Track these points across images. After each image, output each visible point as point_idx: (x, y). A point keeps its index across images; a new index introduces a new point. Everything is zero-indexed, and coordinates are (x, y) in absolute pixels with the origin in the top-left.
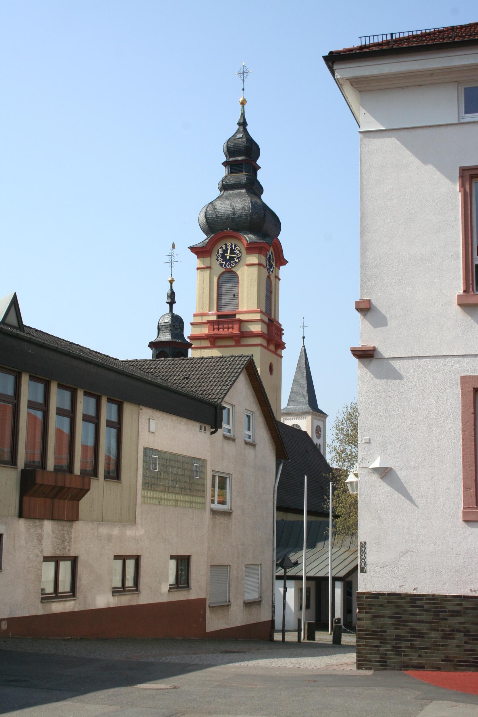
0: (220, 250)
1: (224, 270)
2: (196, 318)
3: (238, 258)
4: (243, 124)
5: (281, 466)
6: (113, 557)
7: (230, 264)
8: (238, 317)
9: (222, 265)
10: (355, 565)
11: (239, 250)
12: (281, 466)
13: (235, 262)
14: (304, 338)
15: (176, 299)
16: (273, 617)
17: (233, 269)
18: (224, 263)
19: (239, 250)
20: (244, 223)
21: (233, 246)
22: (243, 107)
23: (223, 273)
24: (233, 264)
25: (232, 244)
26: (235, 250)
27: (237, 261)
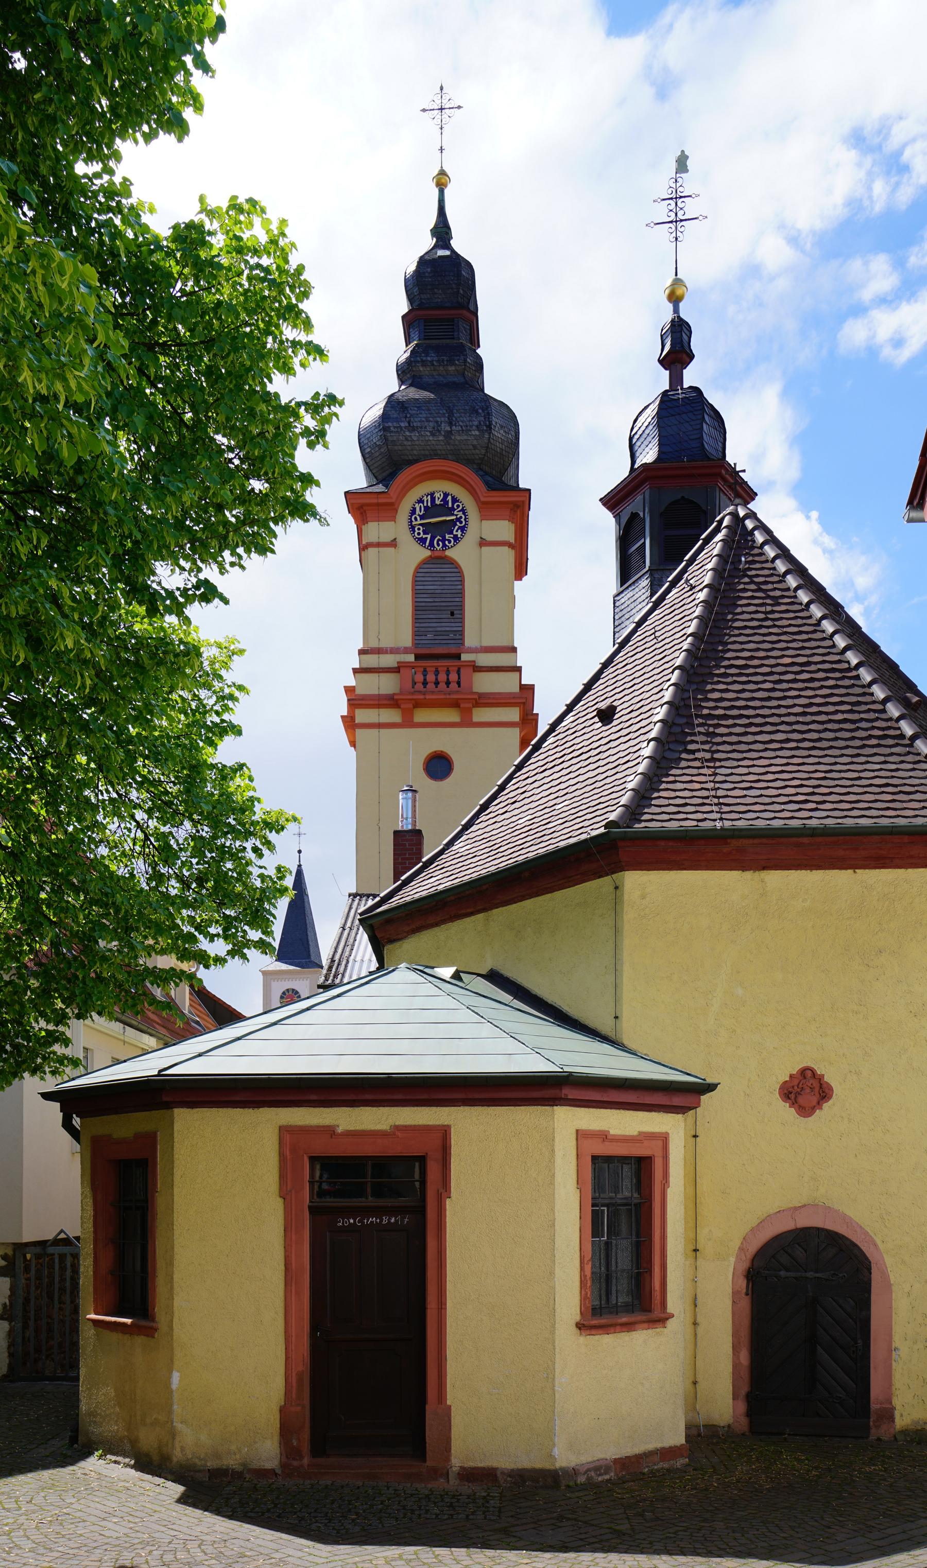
1: (428, 553)
2: (364, 656)
4: (442, 231)
6: (787, 1112)
7: (444, 540)
8: (464, 657)
9: (422, 541)
14: (300, 852)
15: (696, 344)
17: (448, 553)
18: (429, 536)
20: (475, 447)
21: (449, 498)
22: (442, 192)
23: (425, 562)
27: (459, 533)
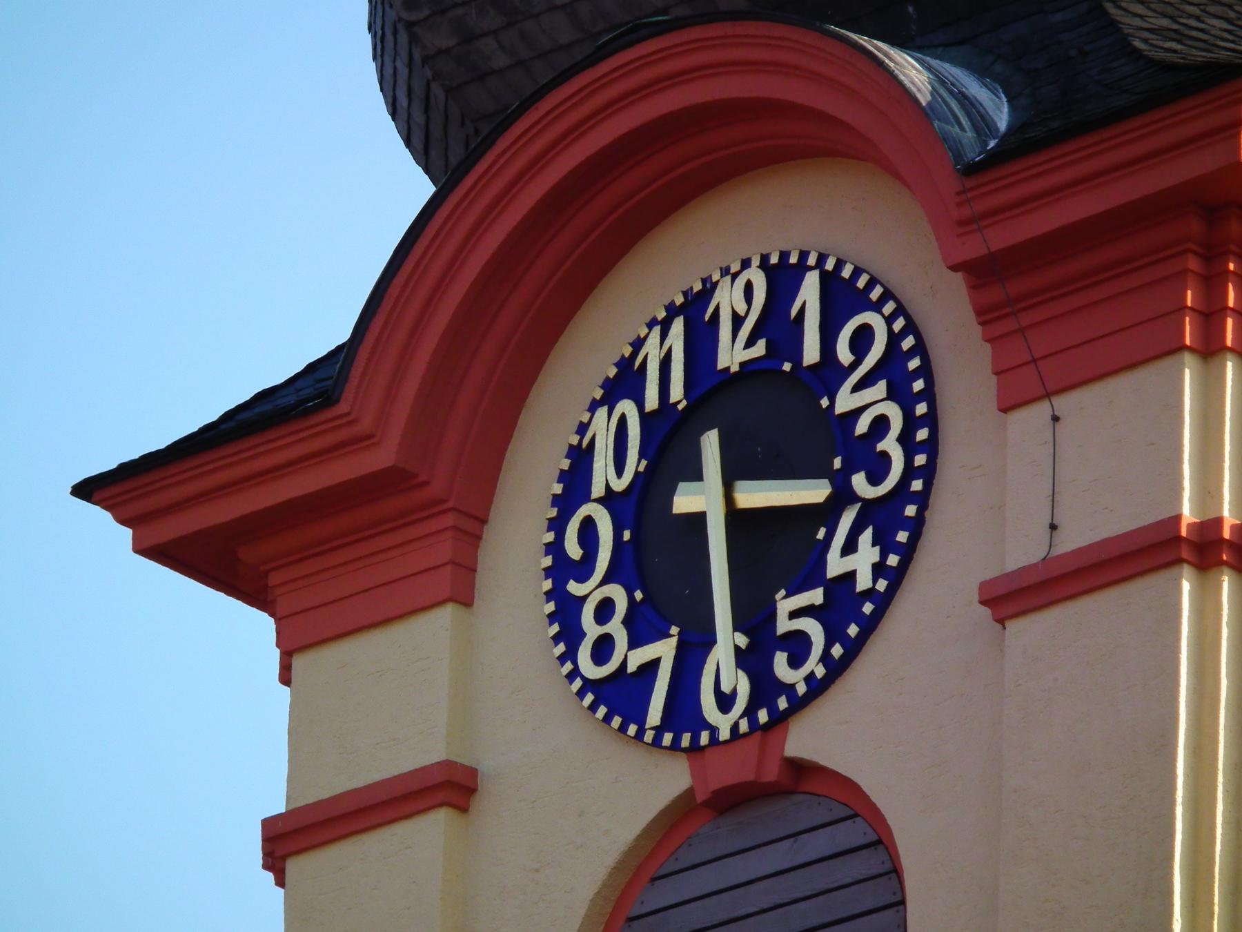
0: (602, 428)
1: (671, 779)
3: (881, 518)
5: (637, 364)
9: (620, 696)
10: (856, 395)
11: (891, 370)
12: (637, 364)
13: (841, 603)
16: (446, 564)
17: (806, 739)
18: (664, 650)
19: (891, 370)
21: (810, 292)
24: (797, 646)
25: (783, 278)
26: (829, 374)
